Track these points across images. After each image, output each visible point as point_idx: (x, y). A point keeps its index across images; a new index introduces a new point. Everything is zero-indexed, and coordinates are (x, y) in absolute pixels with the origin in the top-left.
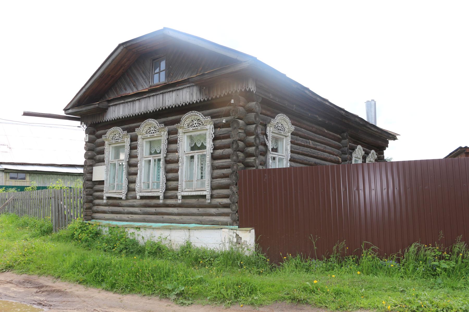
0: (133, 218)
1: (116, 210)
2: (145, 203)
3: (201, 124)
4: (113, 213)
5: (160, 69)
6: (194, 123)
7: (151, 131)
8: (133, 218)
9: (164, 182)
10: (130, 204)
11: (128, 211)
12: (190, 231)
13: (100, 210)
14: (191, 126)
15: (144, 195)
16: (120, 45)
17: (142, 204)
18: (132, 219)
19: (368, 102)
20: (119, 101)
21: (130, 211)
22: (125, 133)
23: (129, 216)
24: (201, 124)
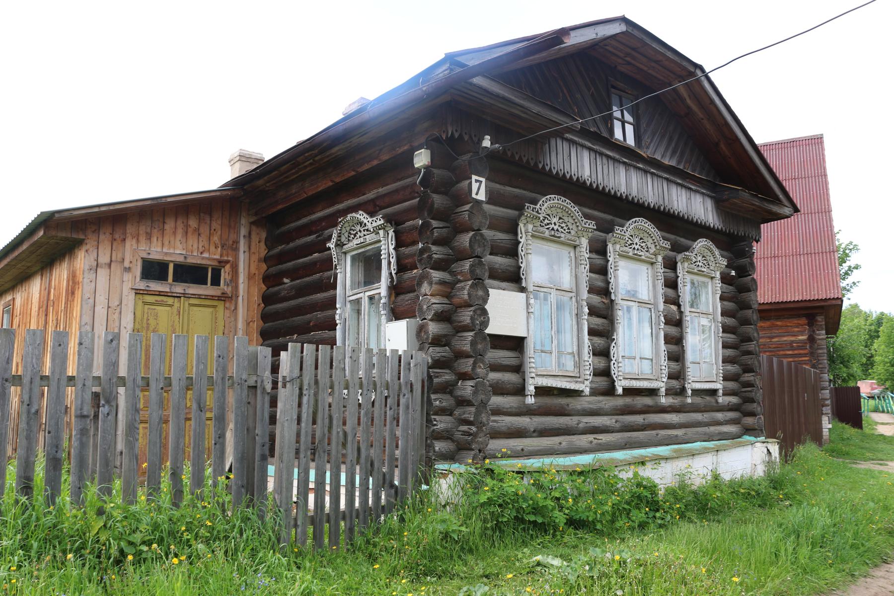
0: (600, 441)
1: (557, 426)
2: (625, 405)
3: (567, 230)
4: (543, 433)
5: (618, 119)
6: (553, 222)
7: (633, 244)
8: (600, 441)
9: (614, 347)
10: (591, 408)
11: (588, 425)
12: (719, 453)
13: (504, 429)
14: (629, 245)
15: (642, 385)
16: (624, 20)
17: (619, 407)
18: (600, 444)
19: (857, 305)
20: (603, 147)
21: (592, 424)
22: (591, 226)
23: (590, 437)
24: (644, 249)
